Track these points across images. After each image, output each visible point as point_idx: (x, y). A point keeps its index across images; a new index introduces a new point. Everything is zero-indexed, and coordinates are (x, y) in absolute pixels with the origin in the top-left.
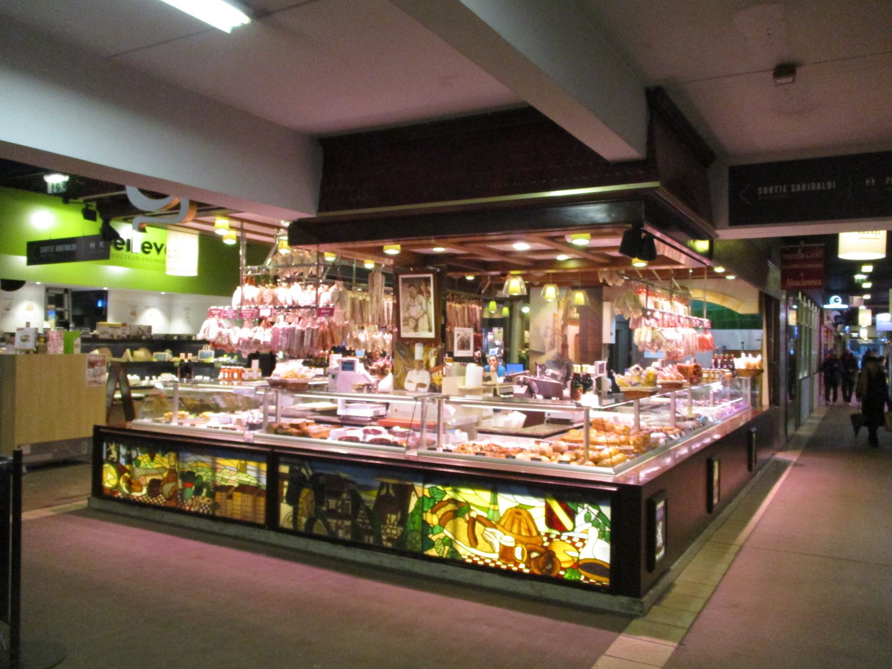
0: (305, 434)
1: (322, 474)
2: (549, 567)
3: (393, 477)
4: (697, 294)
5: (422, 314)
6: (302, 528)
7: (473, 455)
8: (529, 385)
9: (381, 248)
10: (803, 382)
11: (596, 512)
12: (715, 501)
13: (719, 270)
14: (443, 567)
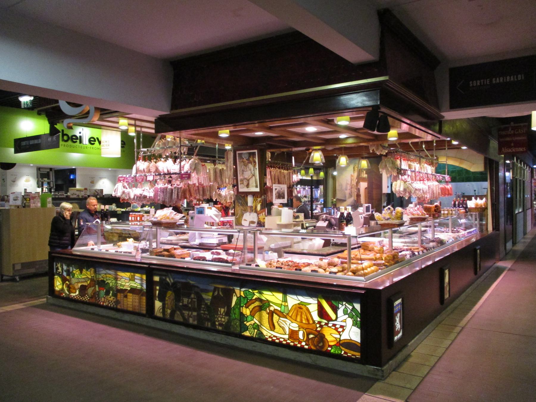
0: (172, 256)
1: (179, 282)
2: (321, 344)
3: (221, 284)
4: (442, 160)
5: (251, 177)
6: (168, 317)
7: (274, 269)
8: (329, 221)
9: (217, 133)
10: (518, 215)
11: (351, 307)
12: (447, 296)
13: (455, 143)
14: (255, 344)
